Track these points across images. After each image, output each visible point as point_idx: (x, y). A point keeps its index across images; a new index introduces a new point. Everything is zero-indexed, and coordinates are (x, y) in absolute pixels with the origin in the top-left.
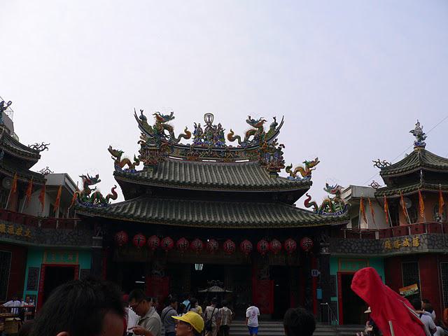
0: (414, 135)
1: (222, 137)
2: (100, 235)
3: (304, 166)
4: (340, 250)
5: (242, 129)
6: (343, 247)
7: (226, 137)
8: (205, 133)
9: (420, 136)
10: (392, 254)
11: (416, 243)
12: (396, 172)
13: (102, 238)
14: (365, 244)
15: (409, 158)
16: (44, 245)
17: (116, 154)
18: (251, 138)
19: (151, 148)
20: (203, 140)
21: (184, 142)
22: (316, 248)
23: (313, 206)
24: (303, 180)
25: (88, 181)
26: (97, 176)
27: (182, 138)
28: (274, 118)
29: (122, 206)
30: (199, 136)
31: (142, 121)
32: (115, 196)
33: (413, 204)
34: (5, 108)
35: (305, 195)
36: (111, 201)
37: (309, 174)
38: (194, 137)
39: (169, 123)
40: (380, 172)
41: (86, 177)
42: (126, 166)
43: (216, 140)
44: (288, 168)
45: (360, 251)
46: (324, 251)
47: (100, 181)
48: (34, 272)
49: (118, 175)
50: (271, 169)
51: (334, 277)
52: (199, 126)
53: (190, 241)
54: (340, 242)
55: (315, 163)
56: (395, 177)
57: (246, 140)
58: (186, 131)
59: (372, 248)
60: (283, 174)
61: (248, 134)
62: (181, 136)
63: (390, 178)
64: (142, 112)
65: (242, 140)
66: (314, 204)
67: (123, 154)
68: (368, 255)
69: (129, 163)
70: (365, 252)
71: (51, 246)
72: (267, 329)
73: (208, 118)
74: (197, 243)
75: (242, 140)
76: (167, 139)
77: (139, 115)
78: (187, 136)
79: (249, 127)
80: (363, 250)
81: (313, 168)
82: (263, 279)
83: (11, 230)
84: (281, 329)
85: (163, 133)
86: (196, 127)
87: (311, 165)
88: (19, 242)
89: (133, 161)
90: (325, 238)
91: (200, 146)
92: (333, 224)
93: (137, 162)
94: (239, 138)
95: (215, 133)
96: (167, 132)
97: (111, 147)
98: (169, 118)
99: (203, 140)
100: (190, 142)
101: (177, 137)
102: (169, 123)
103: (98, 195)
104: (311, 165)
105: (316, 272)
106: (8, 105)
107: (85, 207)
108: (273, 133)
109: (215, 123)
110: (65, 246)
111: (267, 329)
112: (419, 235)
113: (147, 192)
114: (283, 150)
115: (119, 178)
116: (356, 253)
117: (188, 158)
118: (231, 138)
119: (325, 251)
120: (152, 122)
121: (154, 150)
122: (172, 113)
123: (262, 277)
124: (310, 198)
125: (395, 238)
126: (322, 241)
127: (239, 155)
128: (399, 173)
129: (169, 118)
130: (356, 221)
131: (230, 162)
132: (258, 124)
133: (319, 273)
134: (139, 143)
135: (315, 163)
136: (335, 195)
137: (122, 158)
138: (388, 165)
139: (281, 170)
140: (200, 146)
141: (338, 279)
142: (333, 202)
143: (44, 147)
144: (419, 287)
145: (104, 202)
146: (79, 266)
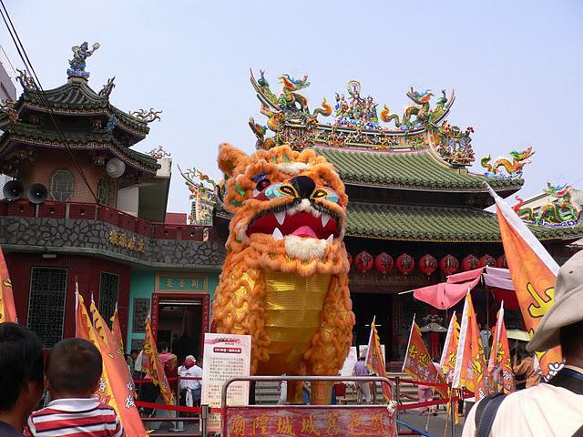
1: (374, 115)
3: (511, 159)
5: (400, 106)
7: (379, 115)
9: (111, 86)
16: (162, 265)
18: (413, 118)
19: (292, 125)
28: (443, 92)
34: (90, 54)
44: (485, 160)
48: (141, 306)
55: (527, 154)
62: (317, 111)
64: (263, 74)
71: (171, 265)
74: (384, 258)
77: (257, 77)
79: (412, 104)
84: (262, 391)
86: (338, 100)
91: (346, 126)
95: (364, 108)
98: (301, 84)
106: (95, 49)
114: (471, 135)
117: (330, 143)
120: (277, 89)
121: (297, 128)
131: (386, 150)
132: (420, 100)
135: (527, 154)
140: (346, 126)
143: (153, 116)
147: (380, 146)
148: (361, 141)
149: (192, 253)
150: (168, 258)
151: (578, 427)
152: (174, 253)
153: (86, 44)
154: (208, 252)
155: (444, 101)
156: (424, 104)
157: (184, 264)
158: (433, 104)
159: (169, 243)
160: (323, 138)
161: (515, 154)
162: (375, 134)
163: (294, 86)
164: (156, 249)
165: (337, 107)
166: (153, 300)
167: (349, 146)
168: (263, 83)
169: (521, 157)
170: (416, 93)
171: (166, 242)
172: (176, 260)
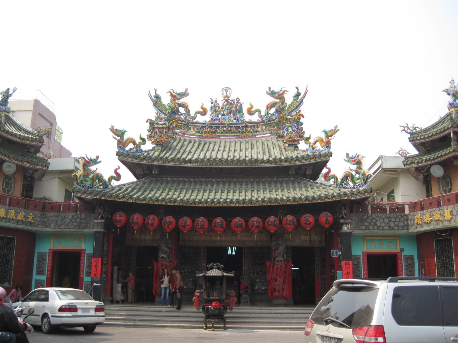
0: (449, 94)
1: (240, 111)
2: (102, 218)
3: (323, 136)
4: (364, 227)
6: (367, 224)
7: (245, 110)
8: (222, 108)
10: (422, 229)
11: (448, 216)
12: (426, 136)
13: (103, 221)
14: (393, 220)
15: (442, 121)
16: (48, 229)
17: (119, 134)
18: (273, 110)
19: (159, 126)
20: (220, 116)
21: (200, 119)
22: (337, 225)
23: (333, 180)
24: (322, 151)
25: (88, 163)
26: (97, 157)
27: (199, 115)
28: (297, 88)
29: (134, 185)
30: (216, 111)
31: (156, 100)
32: (118, 177)
33: (445, 171)
34: (11, 95)
35: (325, 168)
36: (114, 183)
37: (328, 145)
38: (211, 113)
39: (183, 100)
40: (409, 138)
41: (84, 158)
42: (131, 146)
43: (234, 115)
45: (387, 228)
46: (345, 229)
47: (100, 162)
48: (42, 256)
49: (122, 156)
50: (289, 141)
51: (358, 258)
52: (216, 101)
53: (177, 219)
54: (365, 217)
55: (334, 132)
56: (427, 142)
57: (267, 113)
58: (202, 108)
59: (401, 224)
60: (302, 146)
61: (269, 107)
62: (197, 113)
63: (422, 144)
64: (156, 91)
65: (263, 113)
66: (334, 177)
67: (126, 134)
68: (396, 232)
69: (134, 142)
70: (393, 229)
71: (55, 230)
72: (144, 313)
73: (225, 93)
75: (263, 113)
76: (182, 117)
77: (153, 94)
78: (204, 112)
79: (271, 100)
80: (390, 227)
81: (333, 137)
82: (278, 261)
83: (12, 214)
85: (178, 110)
86: (212, 103)
87: (330, 134)
88: (21, 226)
89: (138, 141)
90: (345, 214)
92: (353, 198)
93: (143, 141)
94: (259, 111)
96: (182, 110)
97: (113, 127)
98: (184, 94)
99: (220, 116)
100: (207, 118)
101: (192, 114)
102: (183, 100)
103: (99, 178)
104: (330, 134)
105: (336, 253)
106: (14, 91)
107: (83, 189)
108: (296, 104)
109: (233, 97)
110: (68, 230)
111: (144, 313)
112: (452, 206)
113: (153, 172)
114: (302, 120)
115: (123, 158)
116: (383, 229)
118: (251, 112)
119: (346, 228)
120: (166, 100)
121: (162, 128)
122: (186, 89)
123: (277, 259)
124: (330, 170)
125: (425, 211)
126: (343, 218)
127: (260, 129)
128: (429, 137)
129: (184, 94)
130: (391, 195)
133: (339, 253)
134: (147, 121)
135: (334, 132)
136: (356, 166)
137: (126, 137)
138: (418, 129)
139: (300, 141)
140: (217, 122)
141: (364, 259)
142: (354, 173)
144: (247, 262)
145: (106, 185)
146: (85, 250)
147: (244, 134)
148: (229, 132)
149: (68, 221)
150: (52, 225)
151: (317, 342)
152: (57, 221)
153: (8, 89)
154: (78, 220)
155: (298, 95)
156: (280, 99)
157: (63, 229)
158: (289, 99)
159: (54, 215)
160: (199, 132)
161: (326, 132)
162: (240, 125)
163: (178, 97)
164: (46, 220)
165: (212, 108)
166: (49, 253)
167: (220, 136)
168: (157, 97)
169: (329, 134)
170: (273, 91)
171: (52, 214)
172: (57, 226)
